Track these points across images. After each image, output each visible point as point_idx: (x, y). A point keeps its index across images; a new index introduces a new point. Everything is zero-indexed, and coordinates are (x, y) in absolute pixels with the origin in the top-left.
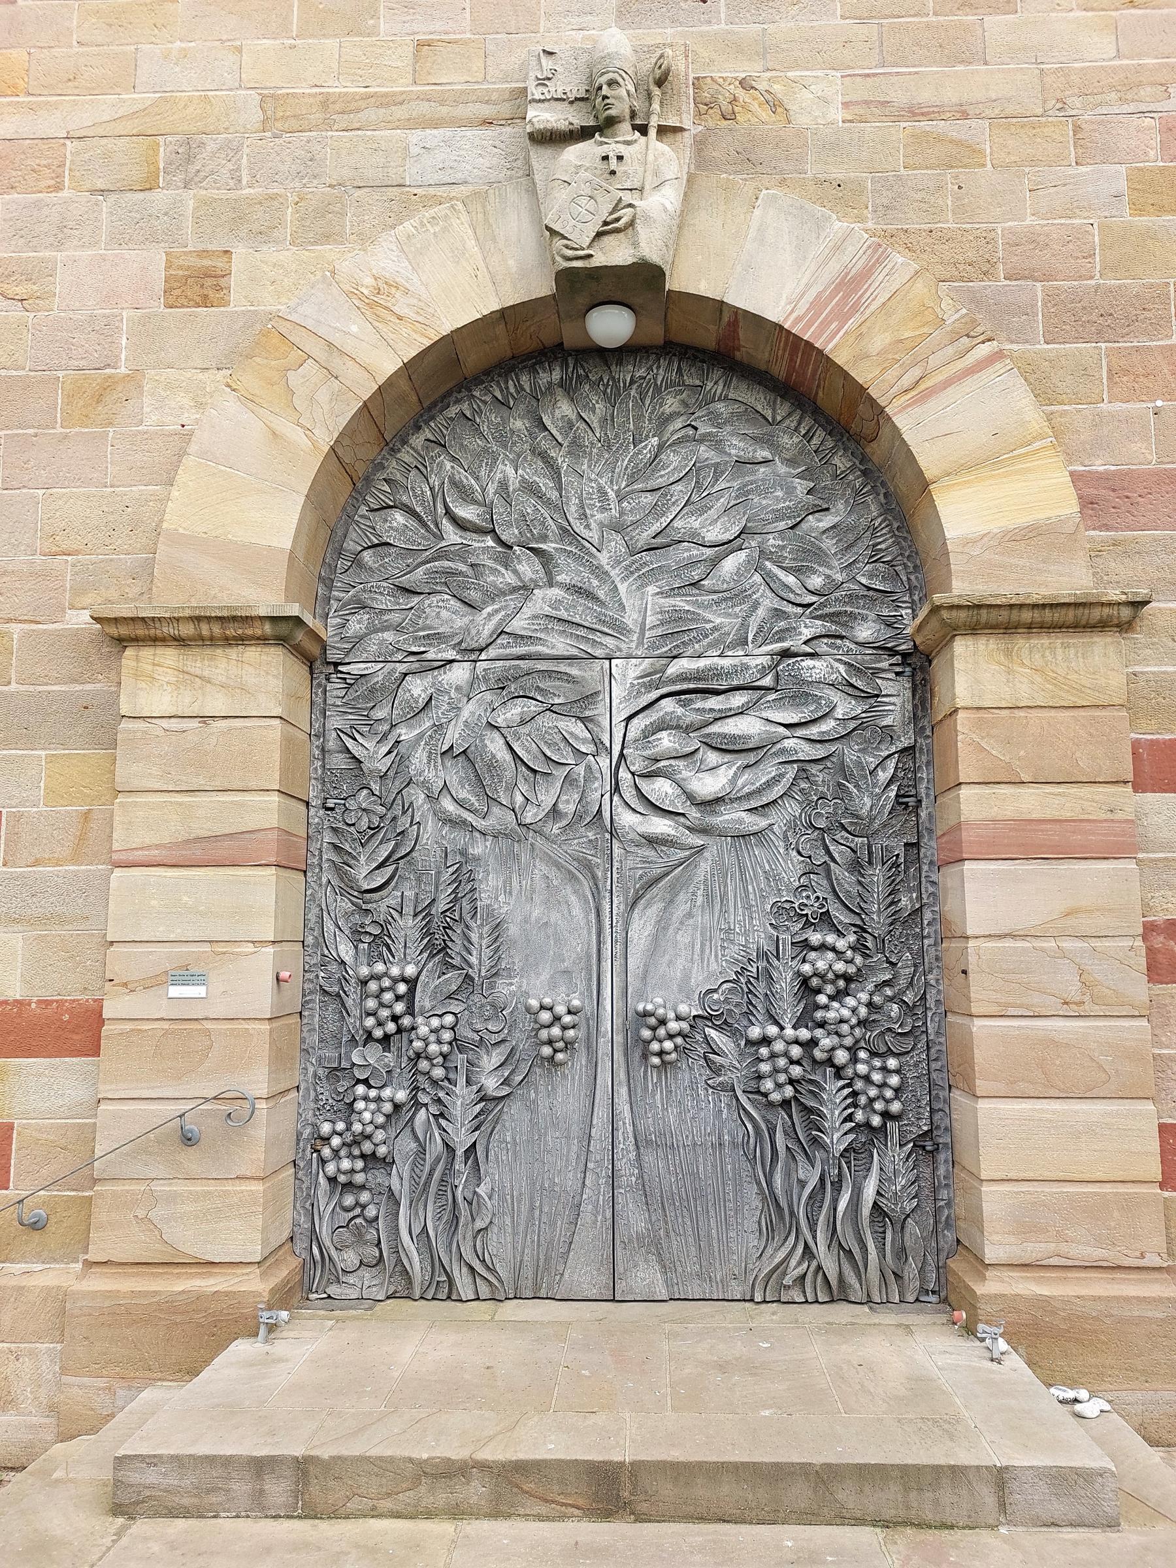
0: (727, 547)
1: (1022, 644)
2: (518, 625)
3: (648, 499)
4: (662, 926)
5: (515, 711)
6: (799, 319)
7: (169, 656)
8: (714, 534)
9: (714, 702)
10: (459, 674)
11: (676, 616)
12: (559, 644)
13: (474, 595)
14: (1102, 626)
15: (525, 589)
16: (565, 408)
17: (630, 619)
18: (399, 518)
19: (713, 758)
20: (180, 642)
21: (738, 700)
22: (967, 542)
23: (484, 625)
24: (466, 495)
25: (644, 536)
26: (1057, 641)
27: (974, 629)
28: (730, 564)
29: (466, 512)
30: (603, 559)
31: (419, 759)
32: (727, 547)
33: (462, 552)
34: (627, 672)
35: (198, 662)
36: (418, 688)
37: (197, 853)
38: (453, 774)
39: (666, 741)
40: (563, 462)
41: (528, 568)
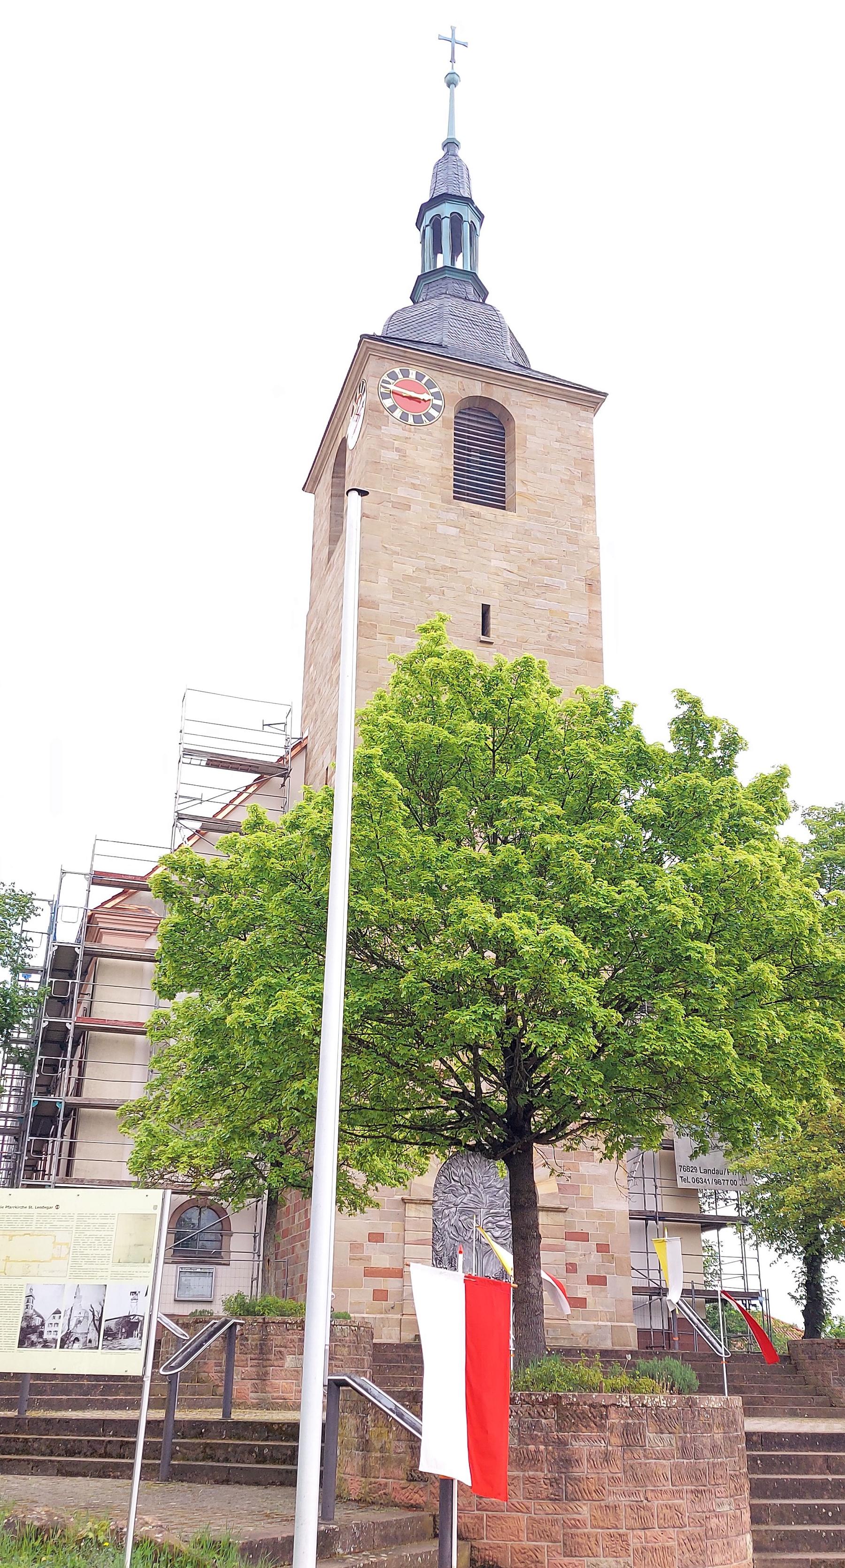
0: (500, 1189)
1: (549, 1213)
2: (464, 1201)
3: (487, 1178)
4: (488, 1260)
5: (464, 1217)
6: (554, 1327)
7: (413, 1205)
8: (498, 1186)
9: (498, 1218)
10: (454, 1209)
11: (492, 1202)
12: (472, 1205)
13: (457, 1195)
14: (561, 1211)
15: (466, 1194)
16: (473, 1159)
17: (484, 1201)
18: (443, 1178)
19: (497, 1229)
20: (416, 1203)
21: (502, 1218)
22: (542, 1195)
23: (458, 1201)
24: (456, 1175)
25: (486, 1185)
26: (555, 1213)
27: (542, 1211)
28: (501, 1192)
29: (456, 1178)
30: (480, 1189)
31: (447, 1226)
32: (500, 1189)
33: (454, 1186)
34: (483, 1211)
35: (418, 1207)
36: (446, 1212)
37: (419, 1242)
38: (452, 1229)
39: (490, 1225)
40: (472, 1169)
41: (466, 1190)
